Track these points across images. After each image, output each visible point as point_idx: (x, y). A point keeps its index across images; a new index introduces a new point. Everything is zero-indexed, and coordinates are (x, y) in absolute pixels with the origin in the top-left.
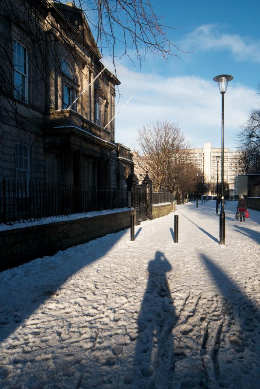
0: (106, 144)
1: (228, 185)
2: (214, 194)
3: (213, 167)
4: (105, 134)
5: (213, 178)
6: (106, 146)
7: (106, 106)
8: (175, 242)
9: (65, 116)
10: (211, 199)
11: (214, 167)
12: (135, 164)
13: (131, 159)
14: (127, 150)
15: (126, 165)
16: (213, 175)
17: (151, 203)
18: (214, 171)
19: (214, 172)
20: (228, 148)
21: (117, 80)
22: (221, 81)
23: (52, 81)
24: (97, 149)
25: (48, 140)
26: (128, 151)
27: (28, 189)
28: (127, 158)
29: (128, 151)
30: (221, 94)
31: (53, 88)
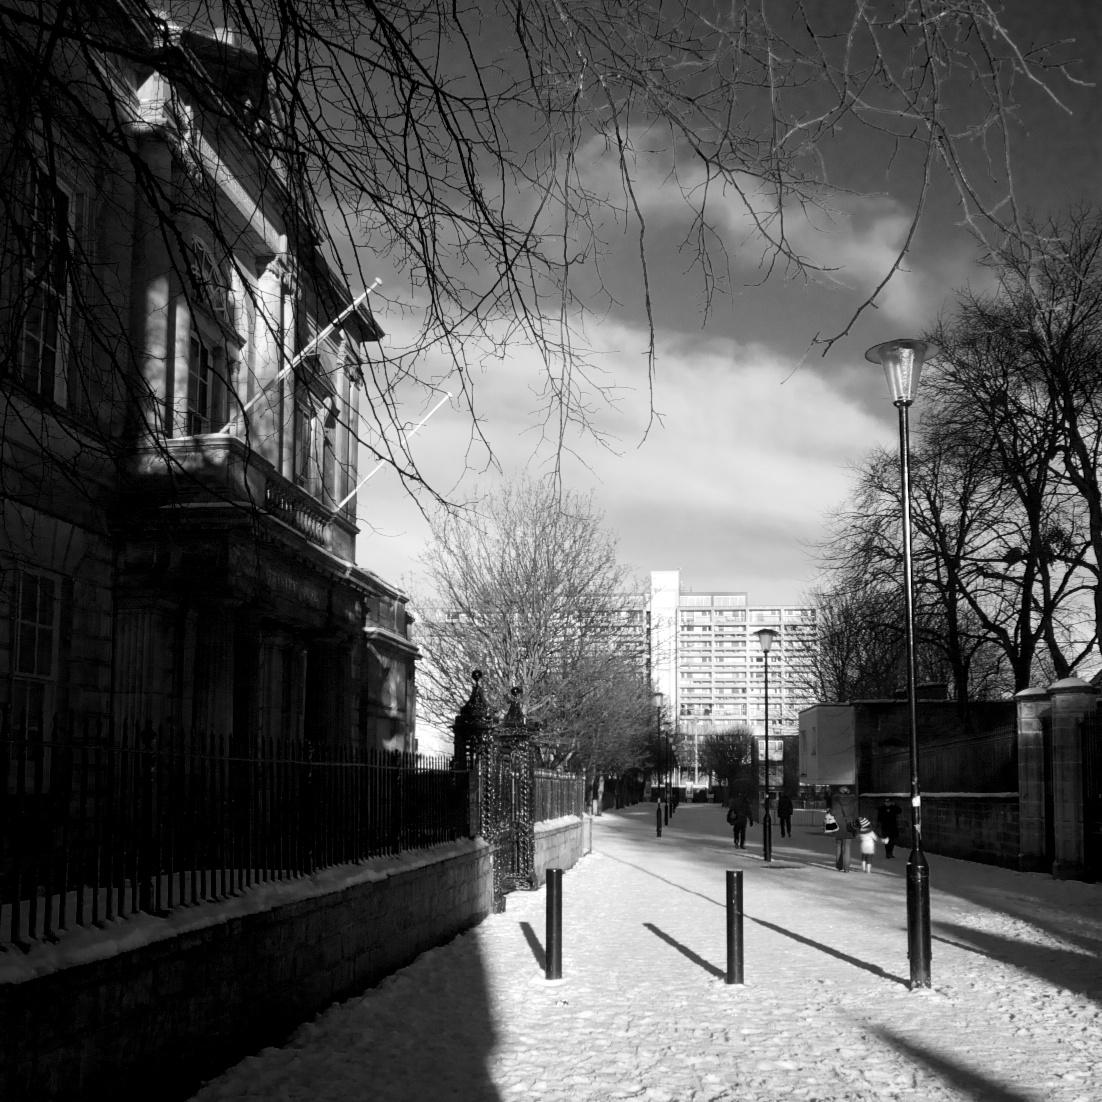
0: (347, 575)
1: (753, 743)
2: (693, 779)
3: (686, 669)
4: (340, 535)
5: (689, 713)
6: (349, 581)
7: (330, 422)
8: (549, 976)
9: (208, 462)
10: (685, 800)
11: (692, 669)
12: (420, 657)
13: (405, 633)
14: (393, 597)
15: (391, 659)
16: (686, 701)
17: (531, 818)
18: (693, 685)
19: (690, 689)
20: (745, 594)
21: (374, 324)
22: (897, 360)
23: (156, 322)
24: (312, 594)
25: (132, 554)
26: (396, 603)
27: (47, 752)
28: (394, 631)
29: (396, 603)
30: (897, 410)
31: (157, 350)
